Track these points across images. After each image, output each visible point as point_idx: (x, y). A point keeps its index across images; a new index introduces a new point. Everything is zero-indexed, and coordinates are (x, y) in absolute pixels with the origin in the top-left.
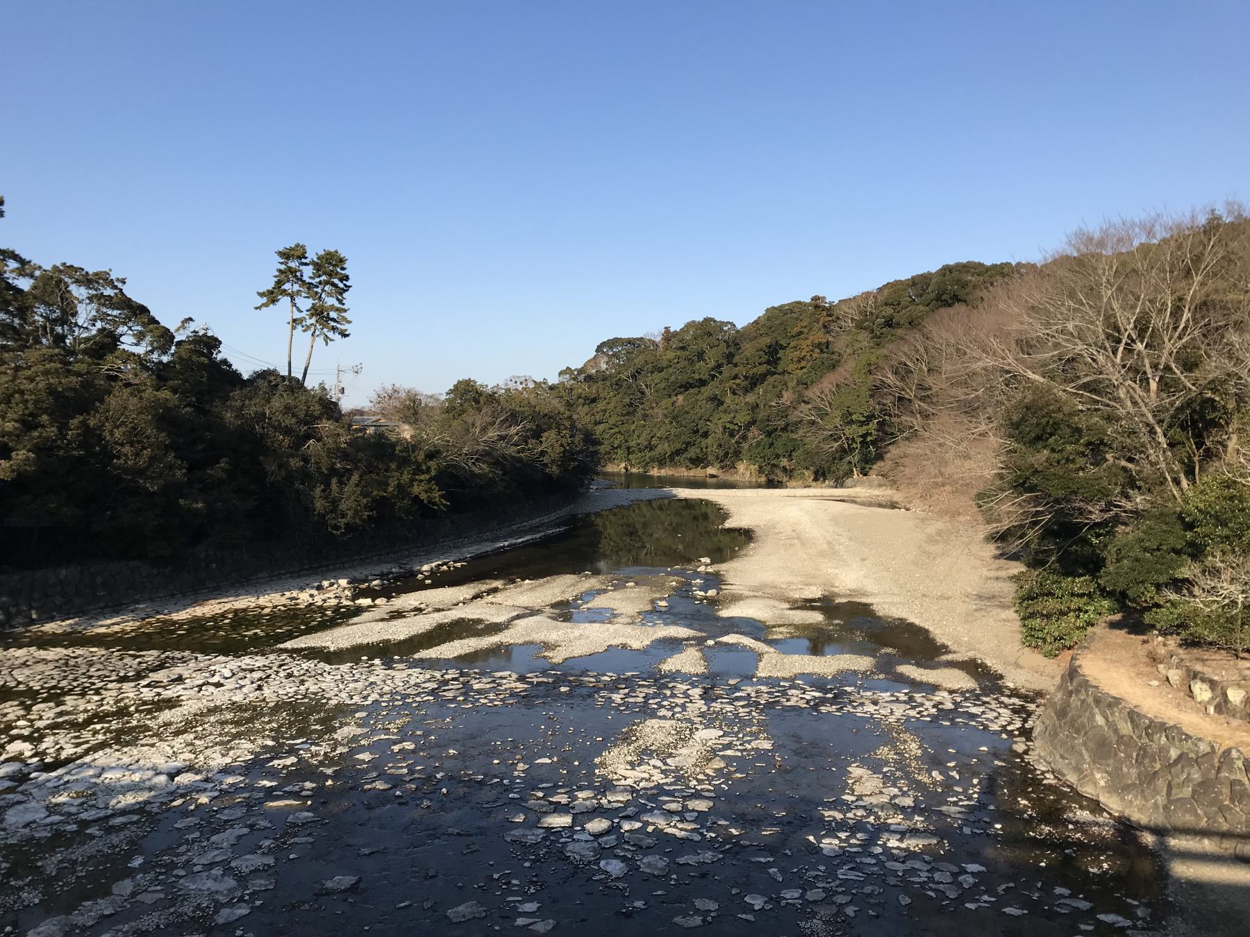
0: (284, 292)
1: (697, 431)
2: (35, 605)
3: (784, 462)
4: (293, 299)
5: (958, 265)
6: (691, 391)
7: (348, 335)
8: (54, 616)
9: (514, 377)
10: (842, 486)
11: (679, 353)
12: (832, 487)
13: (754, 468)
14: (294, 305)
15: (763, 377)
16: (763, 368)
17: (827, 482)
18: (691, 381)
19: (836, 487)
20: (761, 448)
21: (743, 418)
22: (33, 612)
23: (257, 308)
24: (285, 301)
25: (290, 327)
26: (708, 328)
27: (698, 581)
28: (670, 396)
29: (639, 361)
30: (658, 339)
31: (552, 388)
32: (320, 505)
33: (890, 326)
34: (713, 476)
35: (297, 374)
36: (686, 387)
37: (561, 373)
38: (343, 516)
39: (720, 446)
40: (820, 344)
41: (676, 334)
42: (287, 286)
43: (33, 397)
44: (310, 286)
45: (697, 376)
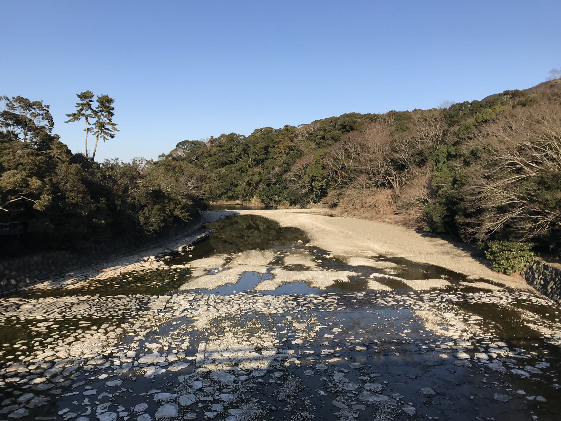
0: (83, 115)
1: (233, 184)
2: (27, 275)
3: (276, 198)
4: (87, 119)
5: (350, 114)
6: (227, 166)
7: (114, 137)
8: (36, 281)
9: (135, 158)
10: (305, 208)
11: (219, 148)
12: (300, 208)
13: (259, 200)
14: (88, 121)
15: (262, 161)
16: (263, 157)
17: (296, 206)
18: (227, 161)
19: (302, 208)
20: (265, 191)
21: (256, 178)
22: (27, 279)
23: (66, 122)
24: (83, 119)
25: (86, 132)
26: (232, 137)
27: (315, 251)
28: (217, 168)
29: (200, 151)
30: (206, 142)
31: (155, 163)
32: (142, 221)
33: (323, 139)
34: (238, 204)
35: (90, 155)
36: (224, 164)
37: (160, 156)
38: (152, 226)
39: (245, 191)
40: (289, 146)
41: (216, 139)
42: (84, 112)
43: (28, 167)
44: (96, 113)
45: (230, 159)
